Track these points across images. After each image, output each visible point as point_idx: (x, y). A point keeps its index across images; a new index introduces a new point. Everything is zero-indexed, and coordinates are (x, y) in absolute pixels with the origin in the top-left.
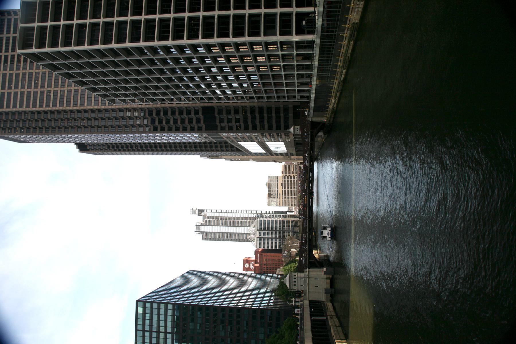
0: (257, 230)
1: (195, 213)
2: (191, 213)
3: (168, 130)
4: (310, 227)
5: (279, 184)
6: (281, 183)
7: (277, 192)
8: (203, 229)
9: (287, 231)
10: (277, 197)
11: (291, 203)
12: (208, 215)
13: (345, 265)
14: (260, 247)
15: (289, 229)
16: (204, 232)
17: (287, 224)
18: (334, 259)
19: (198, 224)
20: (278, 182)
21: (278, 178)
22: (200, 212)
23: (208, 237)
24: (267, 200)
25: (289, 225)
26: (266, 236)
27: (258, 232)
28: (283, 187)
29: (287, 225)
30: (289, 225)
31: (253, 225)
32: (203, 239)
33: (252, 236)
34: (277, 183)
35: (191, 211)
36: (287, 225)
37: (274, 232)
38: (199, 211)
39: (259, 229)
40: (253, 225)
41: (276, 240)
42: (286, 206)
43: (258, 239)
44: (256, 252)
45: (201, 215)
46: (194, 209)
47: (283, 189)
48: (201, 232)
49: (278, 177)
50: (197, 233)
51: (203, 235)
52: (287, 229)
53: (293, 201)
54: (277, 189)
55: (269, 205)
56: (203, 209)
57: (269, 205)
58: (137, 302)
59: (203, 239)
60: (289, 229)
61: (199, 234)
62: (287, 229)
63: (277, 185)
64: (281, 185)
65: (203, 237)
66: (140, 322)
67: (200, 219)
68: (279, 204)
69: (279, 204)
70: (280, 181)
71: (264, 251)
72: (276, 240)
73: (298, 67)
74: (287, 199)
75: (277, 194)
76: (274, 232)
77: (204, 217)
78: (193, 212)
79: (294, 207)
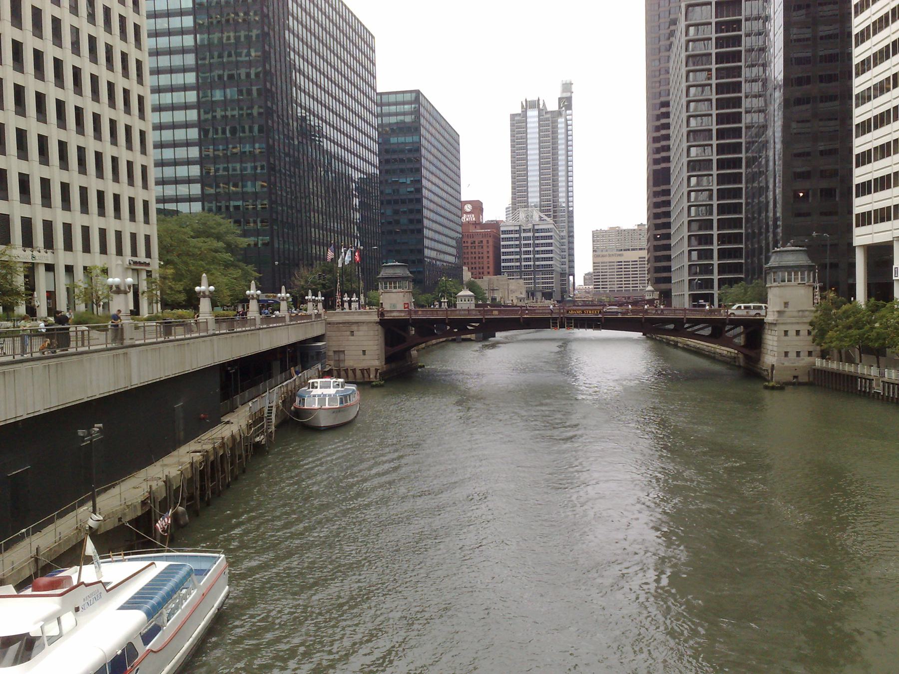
0: (534, 225)
1: (564, 91)
7: (625, 250)
8: (533, 114)
9: (535, 279)
12: (561, 120)
13: (497, 221)
14: (504, 232)
15: (538, 283)
17: (547, 278)
18: (594, 278)
22: (566, 103)
23: (518, 124)
25: (545, 283)
27: (530, 226)
29: (545, 278)
30: (545, 283)
32: (513, 116)
33: (522, 215)
35: (568, 82)
36: (545, 278)
38: (569, 99)
41: (517, 260)
42: (594, 266)
43: (517, 228)
44: (495, 225)
45: (560, 107)
46: (574, 88)
48: (525, 112)
50: (524, 104)
51: (520, 114)
53: (614, 278)
56: (573, 107)
58: (418, 92)
59: (513, 116)
61: (522, 106)
64: (640, 258)
65: (516, 115)
66: (392, 99)
68: (598, 256)
69: (598, 256)
71: (497, 240)
72: (517, 260)
73: (739, 336)
75: (621, 250)
78: (567, 87)
79: (591, 287)
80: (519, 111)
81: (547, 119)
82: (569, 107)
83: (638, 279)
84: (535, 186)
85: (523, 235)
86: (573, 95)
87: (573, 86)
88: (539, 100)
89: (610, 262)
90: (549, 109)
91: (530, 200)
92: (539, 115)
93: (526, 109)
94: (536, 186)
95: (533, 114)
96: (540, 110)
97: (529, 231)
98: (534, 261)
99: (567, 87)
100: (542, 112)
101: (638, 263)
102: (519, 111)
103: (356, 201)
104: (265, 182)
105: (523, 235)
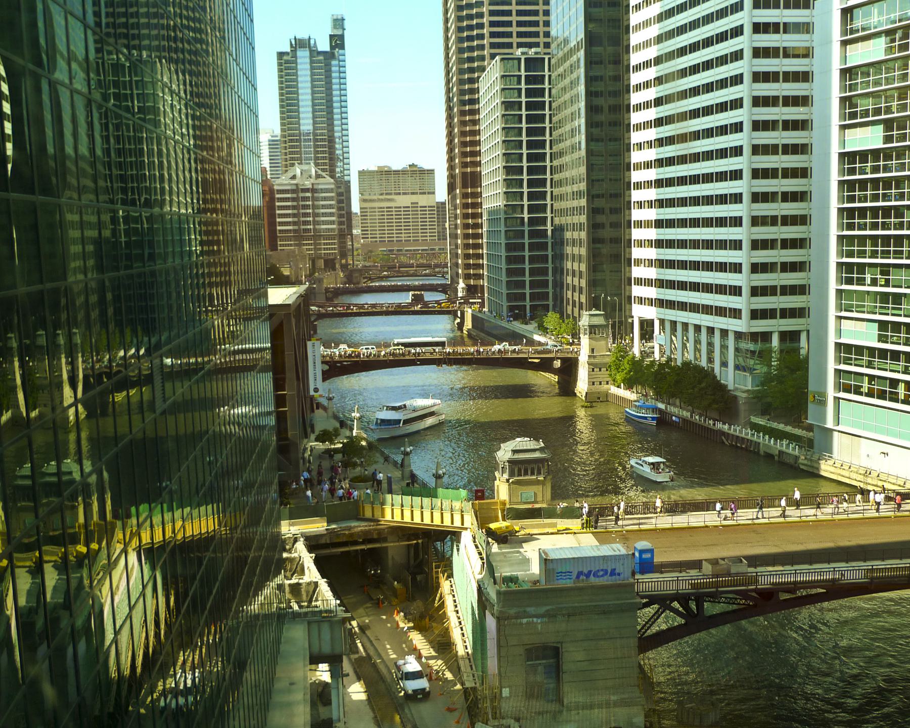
2: (335, 18)
3: (433, 170)
4: (784, 596)
5: (414, 198)
6: (417, 203)
8: (303, 56)
9: (315, 244)
10: (382, 194)
11: (368, 214)
14: (280, 192)
15: (320, 249)
16: (295, 56)
17: (329, 244)
19: (312, 42)
20: (421, 193)
21: (429, 193)
22: (337, 41)
24: (374, 168)
25: (327, 249)
26: (311, 219)
28: (409, 207)
29: (327, 244)
30: (327, 249)
31: (320, 172)
32: (281, 55)
34: (416, 193)
35: (340, 17)
36: (327, 244)
37: (301, 203)
38: (342, 37)
39: (315, 187)
40: (320, 172)
47: (404, 207)
49: (434, 193)
50: (293, 42)
52: (320, 244)
54: (404, 194)
55: (362, 173)
57: (362, 173)
59: (281, 55)
60: (320, 249)
62: (320, 244)
63: (413, 193)
64: (412, 203)
67: (324, 45)
70: (423, 200)
74: (379, 219)
75: (390, 194)
76: (301, 203)
77: (329, 56)
78: (339, 22)
80: (287, 49)
81: (319, 61)
82: (342, 47)
83: (411, 216)
84: (306, 94)
85: (301, 195)
86: (345, 32)
87: (346, 22)
88: (310, 38)
89: (387, 208)
90: (320, 49)
91: (302, 128)
92: (311, 56)
93: (296, 48)
94: (309, 112)
95: (303, 56)
96: (311, 51)
97: (307, 190)
98: (314, 225)
99: (339, 22)
100: (314, 53)
101: (410, 209)
102: (287, 49)
103: (199, 360)
104: (287, 559)
105: (301, 195)
